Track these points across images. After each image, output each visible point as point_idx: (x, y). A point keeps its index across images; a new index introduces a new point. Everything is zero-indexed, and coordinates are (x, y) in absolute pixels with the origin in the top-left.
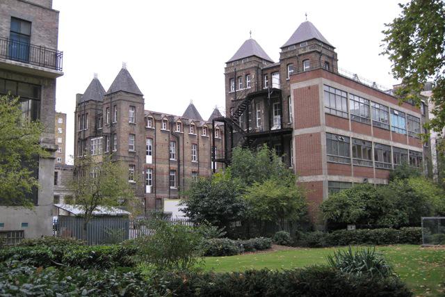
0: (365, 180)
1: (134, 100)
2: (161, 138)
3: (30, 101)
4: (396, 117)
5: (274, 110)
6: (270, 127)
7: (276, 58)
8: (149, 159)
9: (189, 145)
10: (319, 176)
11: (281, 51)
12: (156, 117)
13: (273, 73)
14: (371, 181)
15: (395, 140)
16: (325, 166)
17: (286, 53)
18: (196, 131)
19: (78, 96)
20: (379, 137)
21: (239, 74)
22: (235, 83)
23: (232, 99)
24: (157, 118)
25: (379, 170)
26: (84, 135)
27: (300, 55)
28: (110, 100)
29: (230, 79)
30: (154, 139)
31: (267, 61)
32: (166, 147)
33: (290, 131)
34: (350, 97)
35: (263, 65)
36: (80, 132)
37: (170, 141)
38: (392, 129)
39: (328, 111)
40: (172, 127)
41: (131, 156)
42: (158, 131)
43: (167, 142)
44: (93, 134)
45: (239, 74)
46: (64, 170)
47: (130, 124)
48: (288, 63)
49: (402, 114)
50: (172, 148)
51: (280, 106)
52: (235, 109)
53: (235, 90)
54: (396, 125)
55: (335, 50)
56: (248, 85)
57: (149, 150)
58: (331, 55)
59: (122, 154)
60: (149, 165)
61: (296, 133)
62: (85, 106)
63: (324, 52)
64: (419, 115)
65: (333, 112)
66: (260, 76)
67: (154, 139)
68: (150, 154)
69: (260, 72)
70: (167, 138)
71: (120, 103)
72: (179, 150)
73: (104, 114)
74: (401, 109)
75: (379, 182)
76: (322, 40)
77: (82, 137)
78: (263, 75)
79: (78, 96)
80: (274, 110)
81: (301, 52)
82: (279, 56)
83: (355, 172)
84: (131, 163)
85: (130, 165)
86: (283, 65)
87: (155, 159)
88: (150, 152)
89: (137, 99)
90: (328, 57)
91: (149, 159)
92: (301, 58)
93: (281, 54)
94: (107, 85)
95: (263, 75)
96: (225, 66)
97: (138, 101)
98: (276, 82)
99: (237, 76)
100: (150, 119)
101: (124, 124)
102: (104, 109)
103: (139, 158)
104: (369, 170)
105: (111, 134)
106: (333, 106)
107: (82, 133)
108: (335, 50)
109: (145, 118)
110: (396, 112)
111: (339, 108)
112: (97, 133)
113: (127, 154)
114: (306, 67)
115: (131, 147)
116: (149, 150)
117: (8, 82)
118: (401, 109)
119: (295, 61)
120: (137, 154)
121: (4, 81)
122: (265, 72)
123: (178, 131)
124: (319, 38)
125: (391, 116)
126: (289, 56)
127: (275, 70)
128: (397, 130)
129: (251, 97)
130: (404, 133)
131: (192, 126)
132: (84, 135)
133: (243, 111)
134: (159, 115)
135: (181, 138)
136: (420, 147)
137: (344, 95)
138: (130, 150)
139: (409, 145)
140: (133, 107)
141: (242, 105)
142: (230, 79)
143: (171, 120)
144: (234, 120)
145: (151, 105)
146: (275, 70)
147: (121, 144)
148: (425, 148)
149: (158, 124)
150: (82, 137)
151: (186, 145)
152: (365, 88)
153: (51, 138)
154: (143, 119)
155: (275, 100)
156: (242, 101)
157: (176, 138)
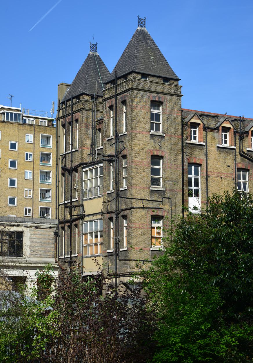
1: (157, 88)
24: (211, 123)
26: (72, 161)
30: (204, 164)
40: (241, 139)
42: (212, 149)
43: (232, 170)
46: (36, 228)
55: (180, 83)
59: (136, 195)
67: (204, 164)
70: (231, 163)
71: (132, 96)
77: (69, 166)
89: (168, 88)
97: (169, 91)
101: (141, 137)
107: (69, 157)
108: (180, 83)
113: (146, 195)
116: (193, 187)
117: (144, 201)
120: (168, 194)
121: (32, 127)
132: (72, 161)
138: (154, 187)
147: (135, 176)
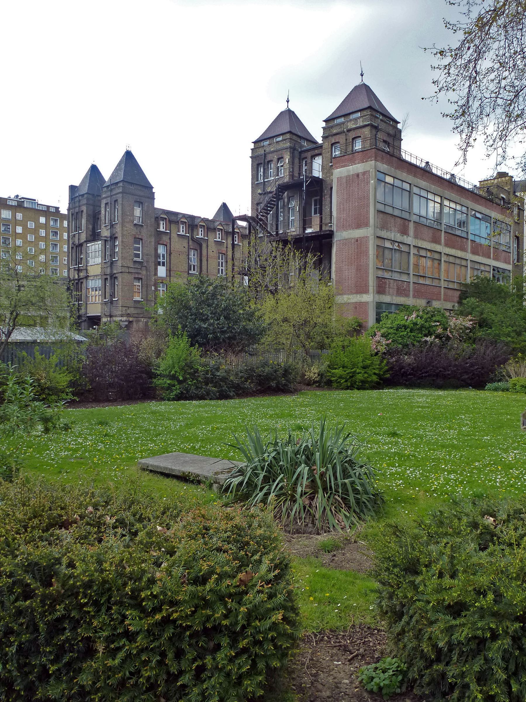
0: (428, 303)
2: (178, 245)
3: (88, 245)
4: (477, 221)
5: (313, 207)
6: (304, 229)
7: (318, 135)
8: (162, 271)
9: (215, 254)
10: (364, 295)
11: (324, 125)
12: (172, 218)
13: (313, 157)
14: (436, 304)
15: (475, 252)
16: (372, 282)
17: (332, 127)
18: (224, 237)
19: (73, 189)
20: (453, 247)
21: (269, 158)
22: (264, 169)
23: (260, 191)
24: (173, 218)
25: (449, 291)
27: (349, 131)
28: (109, 193)
29: (258, 165)
30: (168, 245)
31: (308, 140)
32: (184, 257)
33: (330, 235)
34: (415, 190)
35: (302, 146)
36: (74, 235)
37: (189, 249)
38: (471, 237)
39: (381, 207)
41: (137, 266)
42: (174, 235)
43: (186, 250)
44: (90, 238)
45: (269, 158)
47: (135, 225)
48: (333, 141)
49: (486, 218)
50: (192, 256)
51: (320, 203)
52: (262, 205)
53: (264, 179)
54: (477, 233)
55: (399, 126)
56: (281, 173)
57: (161, 260)
58: (392, 132)
60: (162, 278)
61: (339, 236)
62: (79, 201)
63: (382, 126)
64: (508, 220)
65: (389, 210)
66: (297, 161)
67: (168, 245)
68: (163, 265)
69: (297, 154)
70: (186, 245)
72: (201, 260)
73: (103, 212)
74: (487, 211)
75: (449, 306)
76: (380, 110)
77: (77, 242)
78: (301, 160)
79: (73, 189)
80: (313, 207)
81: (351, 125)
82: (321, 132)
83: (414, 291)
84: (137, 276)
85: (135, 278)
86: (327, 145)
87: (169, 271)
88: (163, 263)
90: (389, 134)
91: (162, 271)
92: (352, 135)
93: (324, 128)
94: (106, 173)
95: (301, 160)
96: (252, 146)
98: (317, 168)
99: (266, 161)
100: (163, 219)
102: (103, 206)
103: (147, 270)
104: (436, 290)
105: (111, 237)
106: (389, 201)
109: (157, 218)
110: (478, 215)
111: (398, 203)
112: (94, 236)
113: (131, 265)
114: (358, 146)
115: (137, 256)
118: (487, 211)
119: (341, 139)
122: (303, 155)
123: (200, 236)
124: (377, 107)
125: (471, 219)
126: (335, 131)
127: (316, 152)
128: (477, 240)
129: (282, 188)
130: (487, 243)
131: (220, 230)
133: (273, 208)
134: (176, 214)
135: (204, 245)
136: (507, 262)
137: (406, 186)
139: (493, 259)
140: (140, 203)
141: (268, 200)
142: (258, 165)
143: (192, 222)
144: (261, 220)
145: (162, 202)
146: (316, 152)
148: (515, 266)
149: (173, 226)
150: (77, 242)
151: (210, 253)
152: (439, 179)
153: (196, 352)
154: (153, 220)
155: (315, 192)
156: (271, 195)
157: (198, 244)
